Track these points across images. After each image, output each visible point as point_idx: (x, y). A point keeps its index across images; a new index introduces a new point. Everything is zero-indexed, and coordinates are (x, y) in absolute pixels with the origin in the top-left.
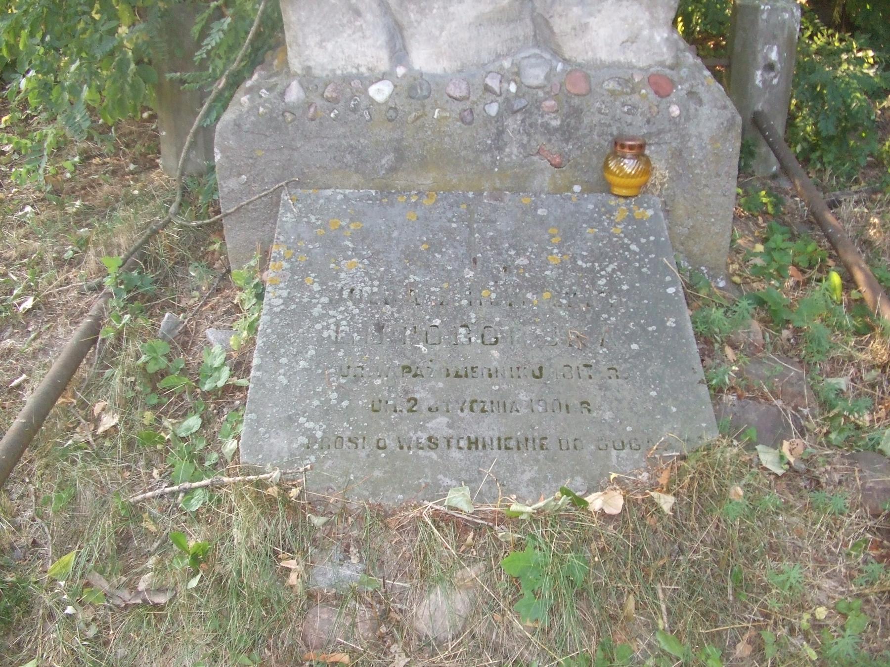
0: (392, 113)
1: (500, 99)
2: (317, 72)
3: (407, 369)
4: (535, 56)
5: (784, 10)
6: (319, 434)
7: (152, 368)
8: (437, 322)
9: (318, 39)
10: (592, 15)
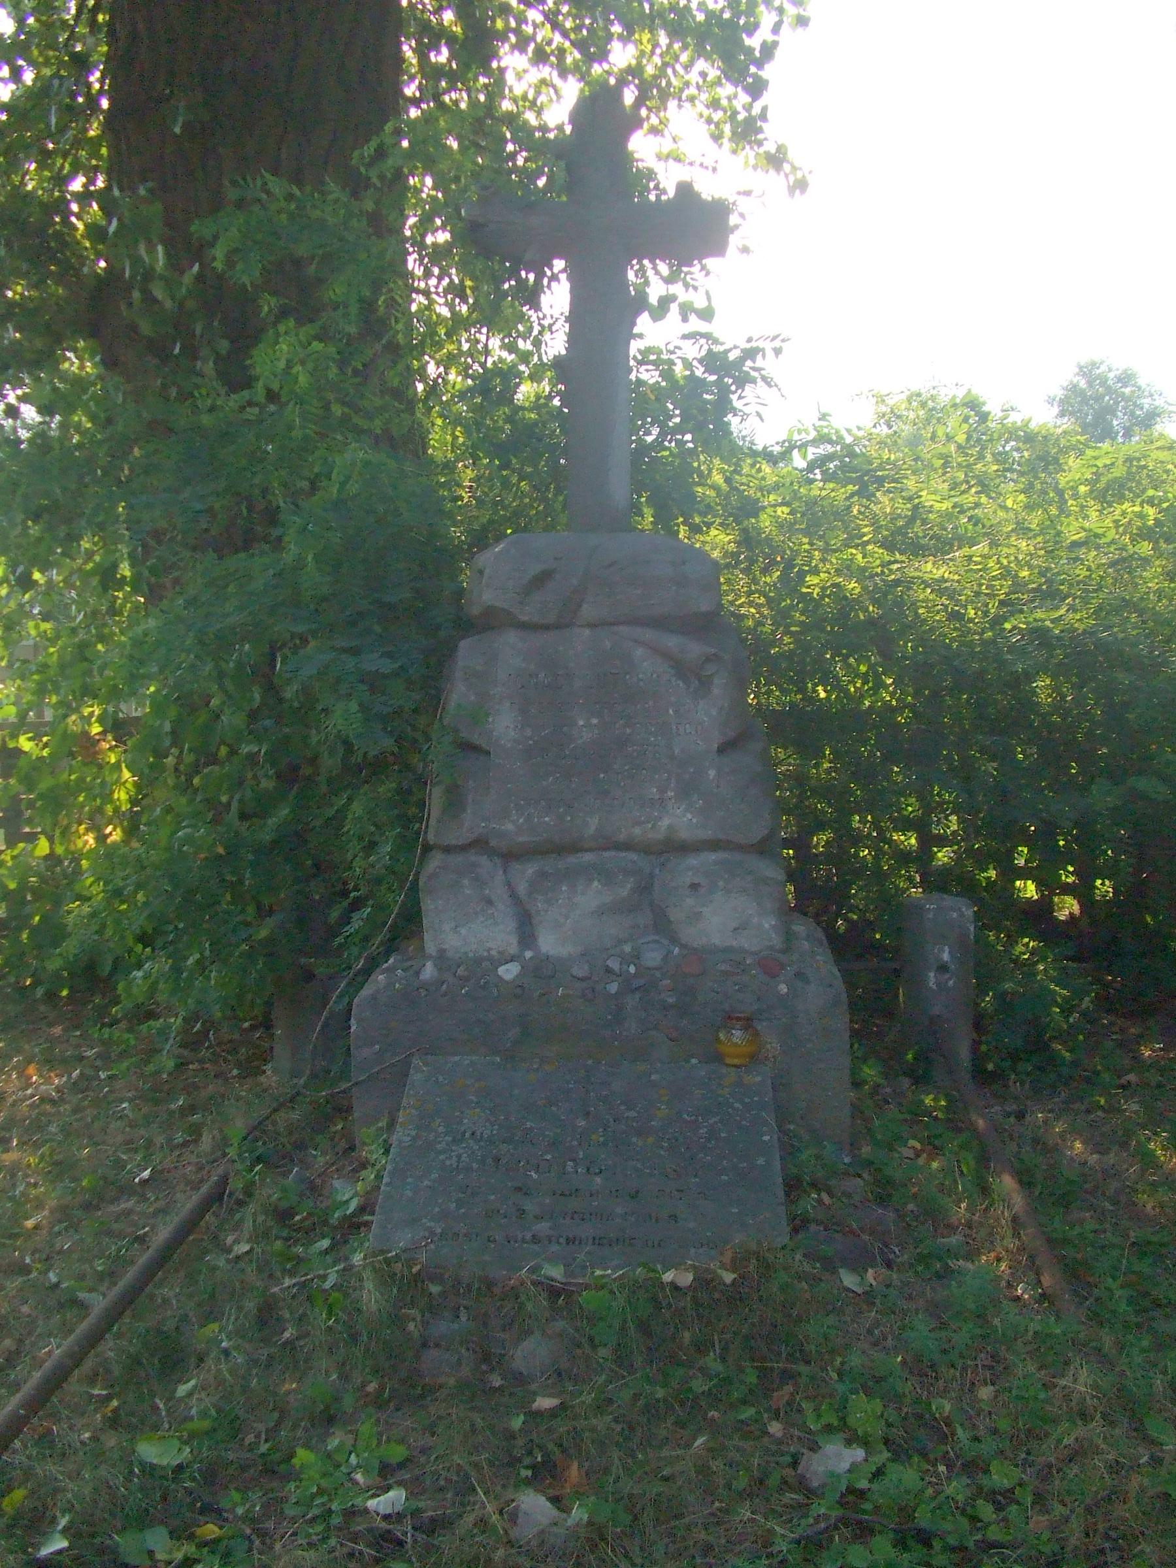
0: (519, 991)
1: (620, 979)
2: (450, 954)
3: (519, 1189)
4: (655, 941)
5: (952, 909)
6: (439, 1230)
7: (284, 1204)
8: (549, 1157)
9: (453, 925)
10: (704, 906)
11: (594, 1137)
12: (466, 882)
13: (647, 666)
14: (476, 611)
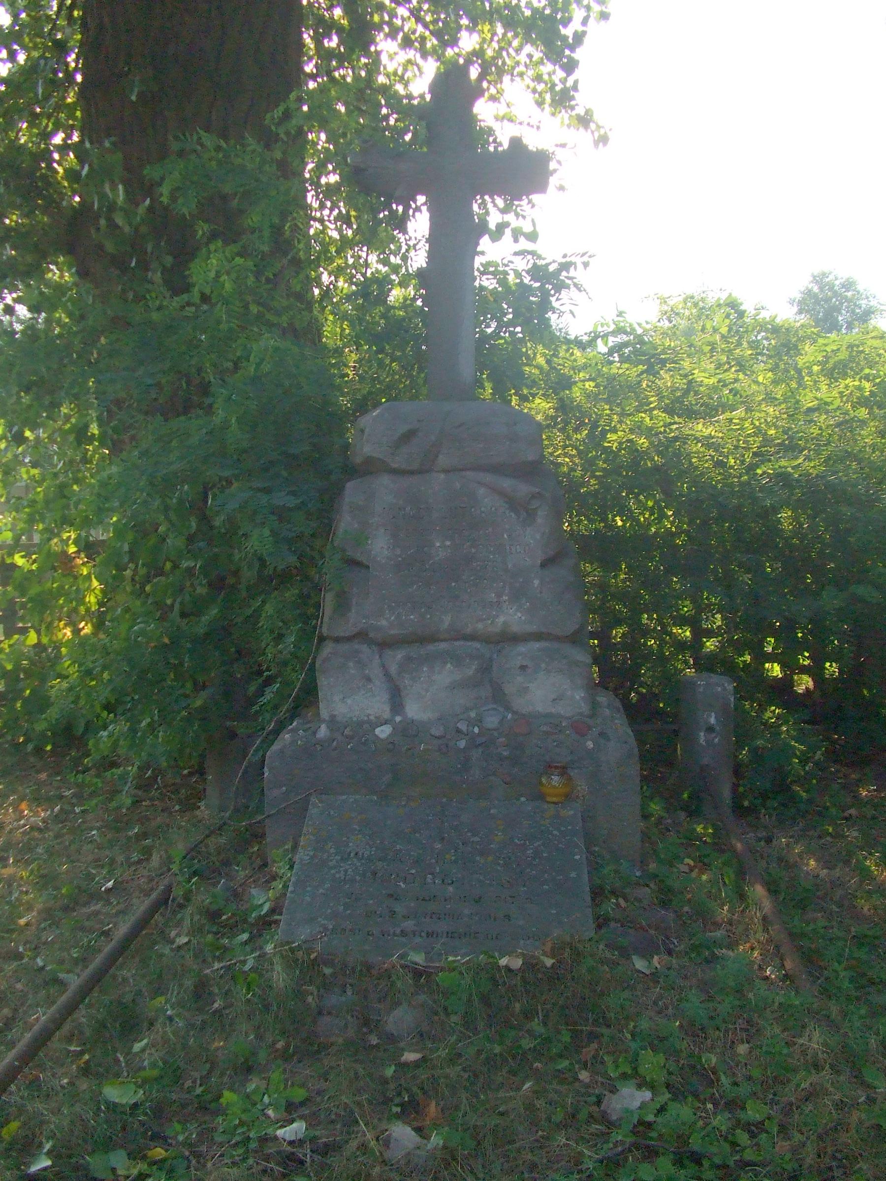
0: (391, 746)
1: (467, 738)
2: (339, 719)
3: (391, 896)
4: (494, 709)
5: (717, 685)
6: (331, 927)
8: (413, 871)
9: (341, 696)
10: (530, 682)
11: (447, 856)
12: (351, 664)
13: (488, 502)
14: (358, 460)
